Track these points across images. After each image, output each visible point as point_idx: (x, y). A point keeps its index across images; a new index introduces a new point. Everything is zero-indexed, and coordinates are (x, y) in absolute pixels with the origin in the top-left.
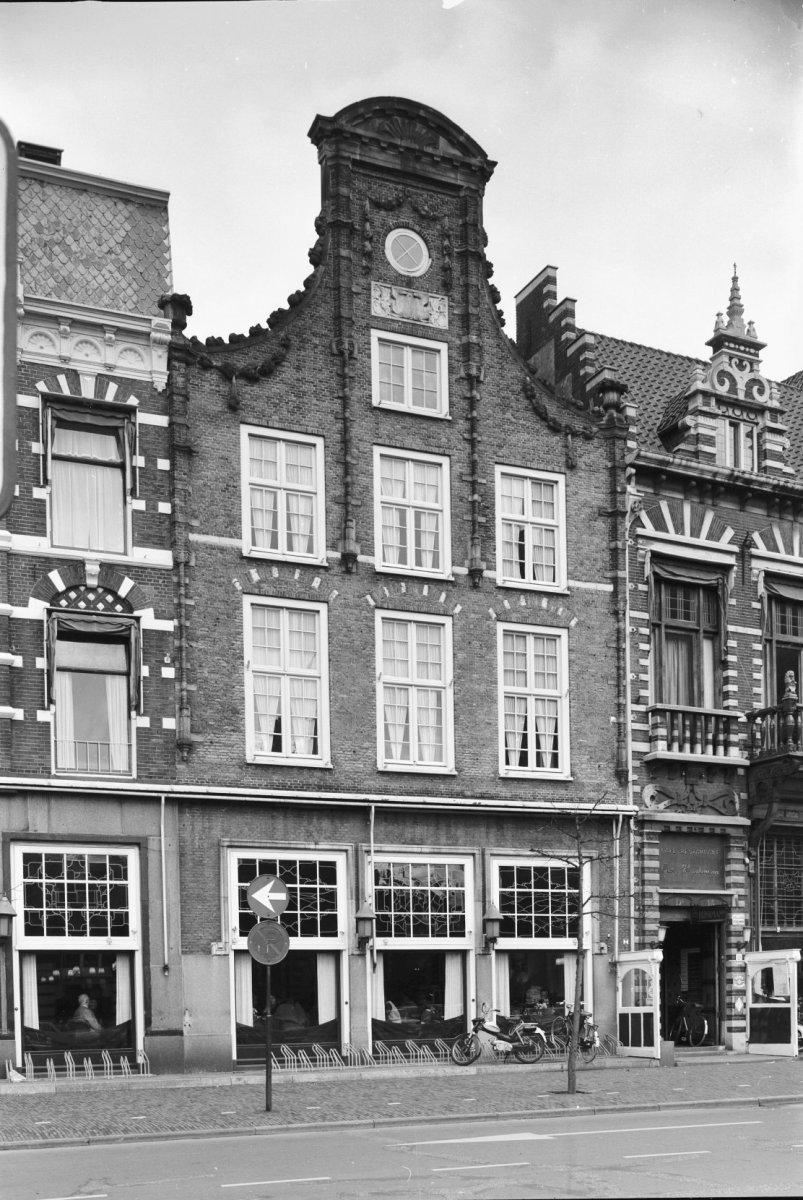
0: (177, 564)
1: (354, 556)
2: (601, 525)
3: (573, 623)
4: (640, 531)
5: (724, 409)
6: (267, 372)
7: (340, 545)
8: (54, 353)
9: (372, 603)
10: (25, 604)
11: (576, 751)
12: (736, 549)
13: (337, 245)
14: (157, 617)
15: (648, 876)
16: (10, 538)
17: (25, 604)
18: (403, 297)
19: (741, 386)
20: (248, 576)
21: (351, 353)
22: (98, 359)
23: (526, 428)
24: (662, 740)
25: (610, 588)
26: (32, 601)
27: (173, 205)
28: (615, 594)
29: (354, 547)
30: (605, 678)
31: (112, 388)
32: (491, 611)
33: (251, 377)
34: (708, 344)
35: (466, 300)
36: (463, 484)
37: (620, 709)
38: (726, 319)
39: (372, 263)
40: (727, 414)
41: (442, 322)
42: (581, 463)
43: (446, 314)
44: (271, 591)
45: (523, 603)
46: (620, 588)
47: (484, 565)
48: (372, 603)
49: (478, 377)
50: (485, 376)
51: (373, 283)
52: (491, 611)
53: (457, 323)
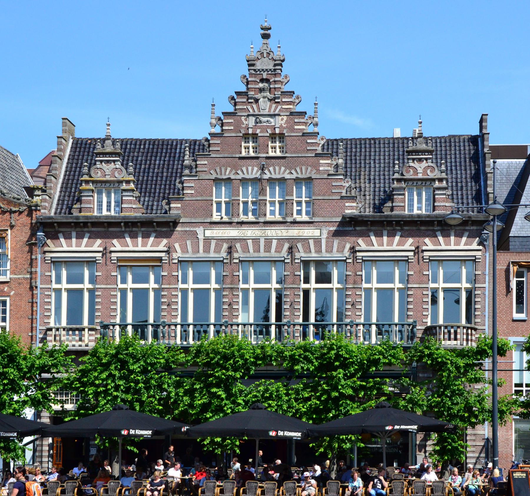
3: (12, 293)
4: (46, 249)
19: (420, 170)
25: (28, 276)
46: (34, 276)
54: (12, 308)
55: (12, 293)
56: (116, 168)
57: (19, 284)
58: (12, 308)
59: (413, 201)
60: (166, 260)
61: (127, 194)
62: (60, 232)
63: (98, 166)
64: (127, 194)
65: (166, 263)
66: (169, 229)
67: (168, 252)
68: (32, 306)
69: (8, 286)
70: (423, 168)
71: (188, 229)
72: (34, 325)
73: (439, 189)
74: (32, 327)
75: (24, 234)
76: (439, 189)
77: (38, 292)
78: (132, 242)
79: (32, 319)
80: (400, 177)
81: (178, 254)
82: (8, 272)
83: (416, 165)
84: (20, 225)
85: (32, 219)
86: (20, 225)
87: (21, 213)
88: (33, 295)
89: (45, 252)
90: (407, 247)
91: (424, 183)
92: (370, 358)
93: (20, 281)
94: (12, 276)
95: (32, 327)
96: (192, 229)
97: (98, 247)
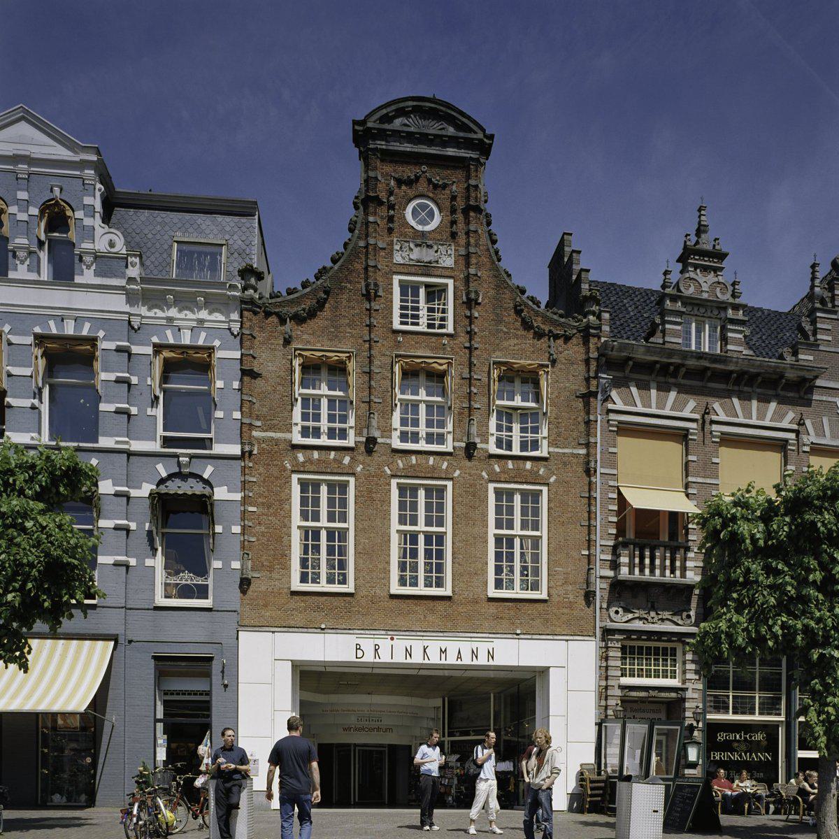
0: (243, 452)
1: (475, 444)
2: (580, 404)
3: (552, 479)
4: (611, 406)
5: (690, 308)
6: (312, 314)
7: (365, 431)
8: (195, 318)
9: (389, 472)
10: (140, 488)
11: (357, 555)
12: (795, 427)
13: (366, 214)
14: (229, 491)
15: (611, 663)
16: (128, 442)
17: (140, 488)
18: (419, 248)
19: (705, 287)
20: (296, 458)
21: (376, 291)
22: (194, 317)
23: (516, 337)
24: (624, 566)
25: (583, 451)
26: (144, 484)
27: (811, 264)
28: (588, 455)
29: (376, 434)
30: (131, 480)
31: (87, 326)
32: (484, 474)
33: (299, 319)
34: (678, 261)
35: (468, 244)
36: (463, 381)
37: (590, 543)
38: (693, 239)
39: (393, 223)
40: (692, 313)
41: (449, 262)
42: (561, 358)
43: (453, 256)
44: (312, 468)
45: (511, 466)
46: (592, 450)
47: (477, 440)
48: (389, 472)
49: (477, 300)
50: (483, 299)
51: (395, 240)
52: (484, 474)
53: (462, 262)
54: (552, 505)
55: (552, 479)
56: (719, 283)
57: (565, 464)
58: (552, 505)
59: (690, 340)
60: (793, 445)
61: (734, 328)
62: (632, 380)
63: (692, 275)
64: (734, 328)
65: (793, 450)
66: (797, 395)
67: (797, 432)
68: (589, 505)
69: (545, 467)
70: (709, 283)
71: (824, 398)
72: (593, 537)
73: (732, 321)
74: (589, 541)
75: (571, 378)
76: (732, 321)
77: (597, 479)
78: (743, 409)
79: (589, 526)
80: (675, 292)
81: (811, 438)
82: (450, 438)
83: (699, 276)
84: (564, 361)
85: (588, 352)
86: (564, 361)
87: (567, 339)
88: (590, 483)
89: (609, 411)
90: (785, 424)
91: (696, 309)
92: (75, 580)
93: (565, 459)
94: (551, 449)
95: (589, 541)
96: (830, 399)
97: (691, 412)
